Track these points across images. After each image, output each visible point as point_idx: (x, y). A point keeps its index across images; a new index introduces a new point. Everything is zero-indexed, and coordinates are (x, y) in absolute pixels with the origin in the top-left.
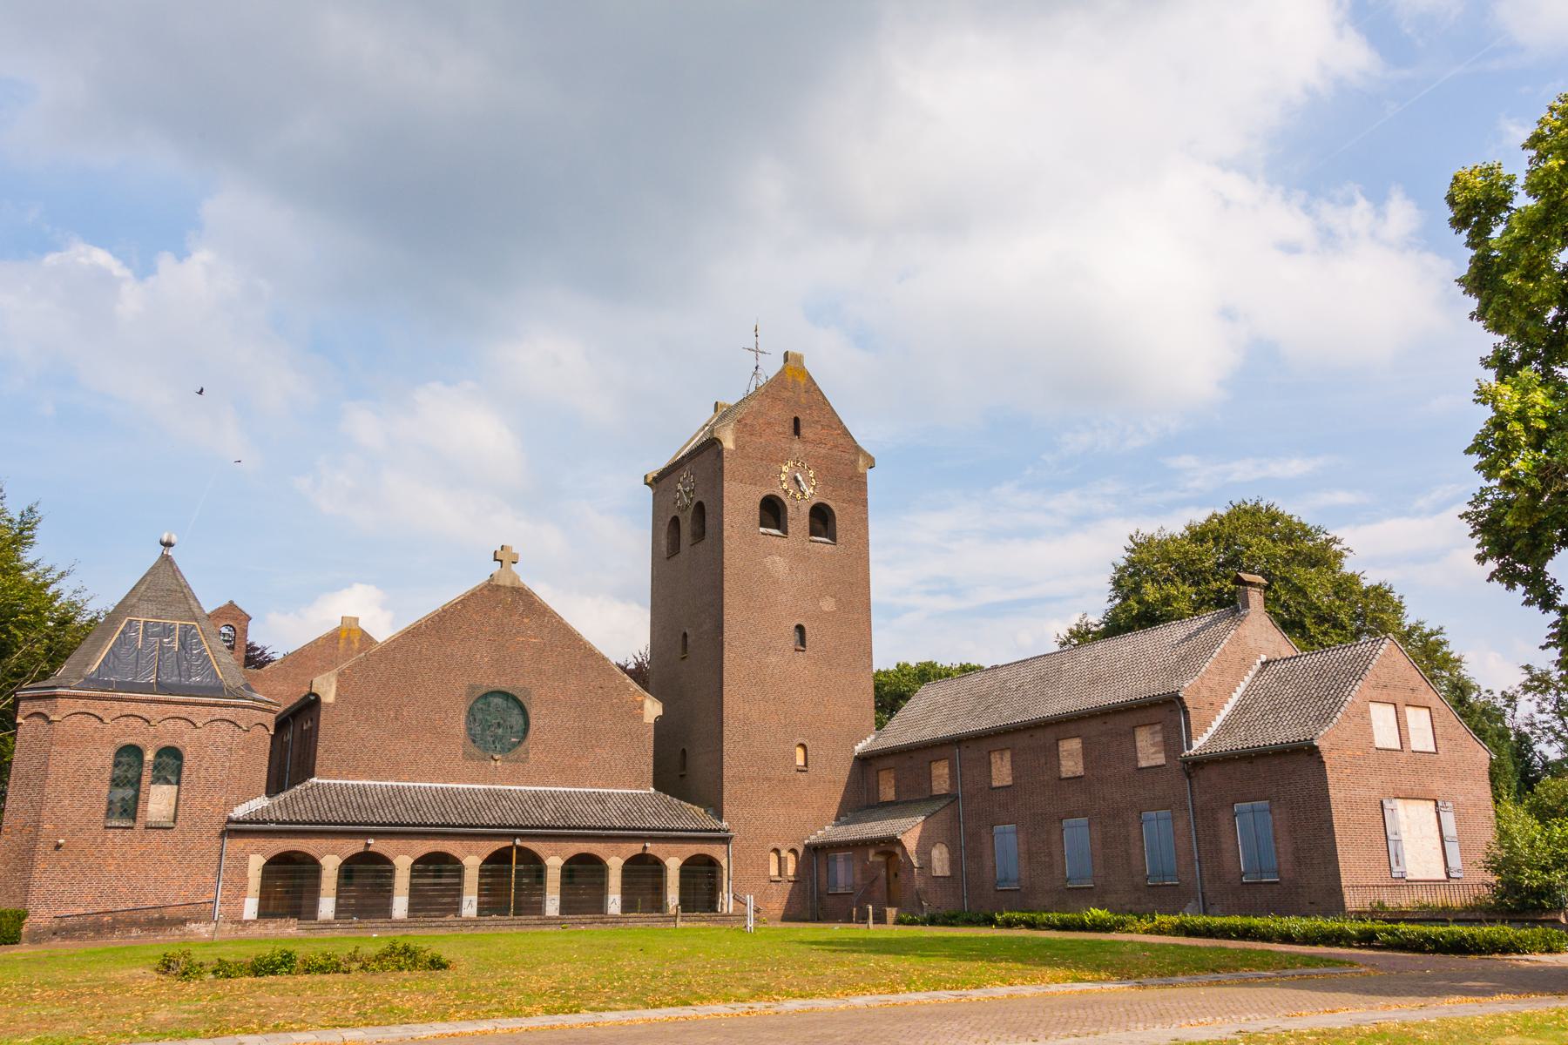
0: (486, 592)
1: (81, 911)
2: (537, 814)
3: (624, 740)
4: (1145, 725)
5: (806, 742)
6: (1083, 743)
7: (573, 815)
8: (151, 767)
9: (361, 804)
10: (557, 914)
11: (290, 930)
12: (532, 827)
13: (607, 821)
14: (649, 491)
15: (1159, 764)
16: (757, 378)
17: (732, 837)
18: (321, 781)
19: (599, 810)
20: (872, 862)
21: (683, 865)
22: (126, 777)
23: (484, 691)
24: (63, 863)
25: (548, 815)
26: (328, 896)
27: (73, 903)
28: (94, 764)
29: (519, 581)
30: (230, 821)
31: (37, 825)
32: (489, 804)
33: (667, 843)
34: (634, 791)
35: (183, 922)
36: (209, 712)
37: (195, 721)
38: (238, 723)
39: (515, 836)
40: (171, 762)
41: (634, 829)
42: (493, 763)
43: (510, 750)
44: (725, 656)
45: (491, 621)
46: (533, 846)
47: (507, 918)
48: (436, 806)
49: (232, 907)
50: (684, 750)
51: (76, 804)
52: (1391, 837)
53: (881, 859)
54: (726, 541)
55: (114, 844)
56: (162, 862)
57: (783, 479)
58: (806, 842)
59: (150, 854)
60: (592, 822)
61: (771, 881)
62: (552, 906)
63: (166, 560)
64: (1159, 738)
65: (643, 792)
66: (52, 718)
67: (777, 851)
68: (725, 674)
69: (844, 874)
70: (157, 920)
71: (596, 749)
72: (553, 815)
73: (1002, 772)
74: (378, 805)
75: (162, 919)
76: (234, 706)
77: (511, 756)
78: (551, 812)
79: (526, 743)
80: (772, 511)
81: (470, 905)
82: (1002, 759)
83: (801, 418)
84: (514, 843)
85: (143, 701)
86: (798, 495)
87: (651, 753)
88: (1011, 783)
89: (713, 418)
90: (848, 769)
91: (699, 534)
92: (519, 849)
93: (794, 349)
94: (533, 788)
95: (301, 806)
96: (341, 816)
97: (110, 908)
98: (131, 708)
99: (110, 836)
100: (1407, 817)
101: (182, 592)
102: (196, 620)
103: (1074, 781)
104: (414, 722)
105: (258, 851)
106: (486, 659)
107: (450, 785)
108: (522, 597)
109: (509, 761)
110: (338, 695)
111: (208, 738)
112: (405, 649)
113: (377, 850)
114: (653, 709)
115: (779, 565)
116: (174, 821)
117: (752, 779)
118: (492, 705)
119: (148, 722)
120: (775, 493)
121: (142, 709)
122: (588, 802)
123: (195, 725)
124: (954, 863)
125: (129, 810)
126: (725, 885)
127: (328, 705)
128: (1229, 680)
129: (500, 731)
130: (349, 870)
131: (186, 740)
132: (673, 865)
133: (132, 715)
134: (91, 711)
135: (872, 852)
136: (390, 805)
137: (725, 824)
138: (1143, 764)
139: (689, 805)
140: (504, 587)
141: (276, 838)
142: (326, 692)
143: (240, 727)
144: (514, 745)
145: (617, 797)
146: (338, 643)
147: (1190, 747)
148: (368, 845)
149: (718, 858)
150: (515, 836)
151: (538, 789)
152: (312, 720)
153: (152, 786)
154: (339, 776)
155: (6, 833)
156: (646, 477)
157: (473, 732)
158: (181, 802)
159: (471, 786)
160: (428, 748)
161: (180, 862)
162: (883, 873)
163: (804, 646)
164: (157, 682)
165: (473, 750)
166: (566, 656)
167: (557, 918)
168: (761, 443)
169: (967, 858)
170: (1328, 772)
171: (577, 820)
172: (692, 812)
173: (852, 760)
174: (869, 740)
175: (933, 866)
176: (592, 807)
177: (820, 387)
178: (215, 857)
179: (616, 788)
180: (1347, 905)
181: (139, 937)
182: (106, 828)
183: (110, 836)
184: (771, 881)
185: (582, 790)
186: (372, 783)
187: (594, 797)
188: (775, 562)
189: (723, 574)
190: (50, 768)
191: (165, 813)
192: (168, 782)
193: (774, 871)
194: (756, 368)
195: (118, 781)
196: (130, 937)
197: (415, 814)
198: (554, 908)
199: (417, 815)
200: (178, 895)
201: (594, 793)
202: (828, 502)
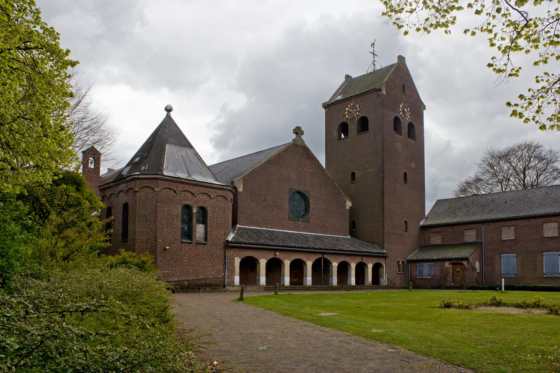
20: (447, 267)
26: (263, 276)
28: (174, 212)
30: (228, 241)
31: (156, 239)
37: (211, 195)
38: (227, 197)
39: (323, 253)
49: (230, 280)
51: (170, 231)
53: (450, 266)
62: (309, 280)
63: (169, 118)
66: (156, 189)
75: (206, 284)
76: (225, 190)
82: (509, 230)
83: (405, 85)
110: (243, 188)
111: (216, 204)
115: (399, 146)
125: (188, 234)
127: (240, 192)
130: (292, 265)
131: (208, 204)
133: (187, 191)
134: (171, 187)
137: (385, 251)
143: (227, 199)
150: (323, 253)
155: (138, 242)
161: (210, 260)
162: (451, 271)
163: (407, 181)
169: (485, 266)
173: (419, 227)
178: (223, 258)
188: (398, 145)
198: (335, 283)
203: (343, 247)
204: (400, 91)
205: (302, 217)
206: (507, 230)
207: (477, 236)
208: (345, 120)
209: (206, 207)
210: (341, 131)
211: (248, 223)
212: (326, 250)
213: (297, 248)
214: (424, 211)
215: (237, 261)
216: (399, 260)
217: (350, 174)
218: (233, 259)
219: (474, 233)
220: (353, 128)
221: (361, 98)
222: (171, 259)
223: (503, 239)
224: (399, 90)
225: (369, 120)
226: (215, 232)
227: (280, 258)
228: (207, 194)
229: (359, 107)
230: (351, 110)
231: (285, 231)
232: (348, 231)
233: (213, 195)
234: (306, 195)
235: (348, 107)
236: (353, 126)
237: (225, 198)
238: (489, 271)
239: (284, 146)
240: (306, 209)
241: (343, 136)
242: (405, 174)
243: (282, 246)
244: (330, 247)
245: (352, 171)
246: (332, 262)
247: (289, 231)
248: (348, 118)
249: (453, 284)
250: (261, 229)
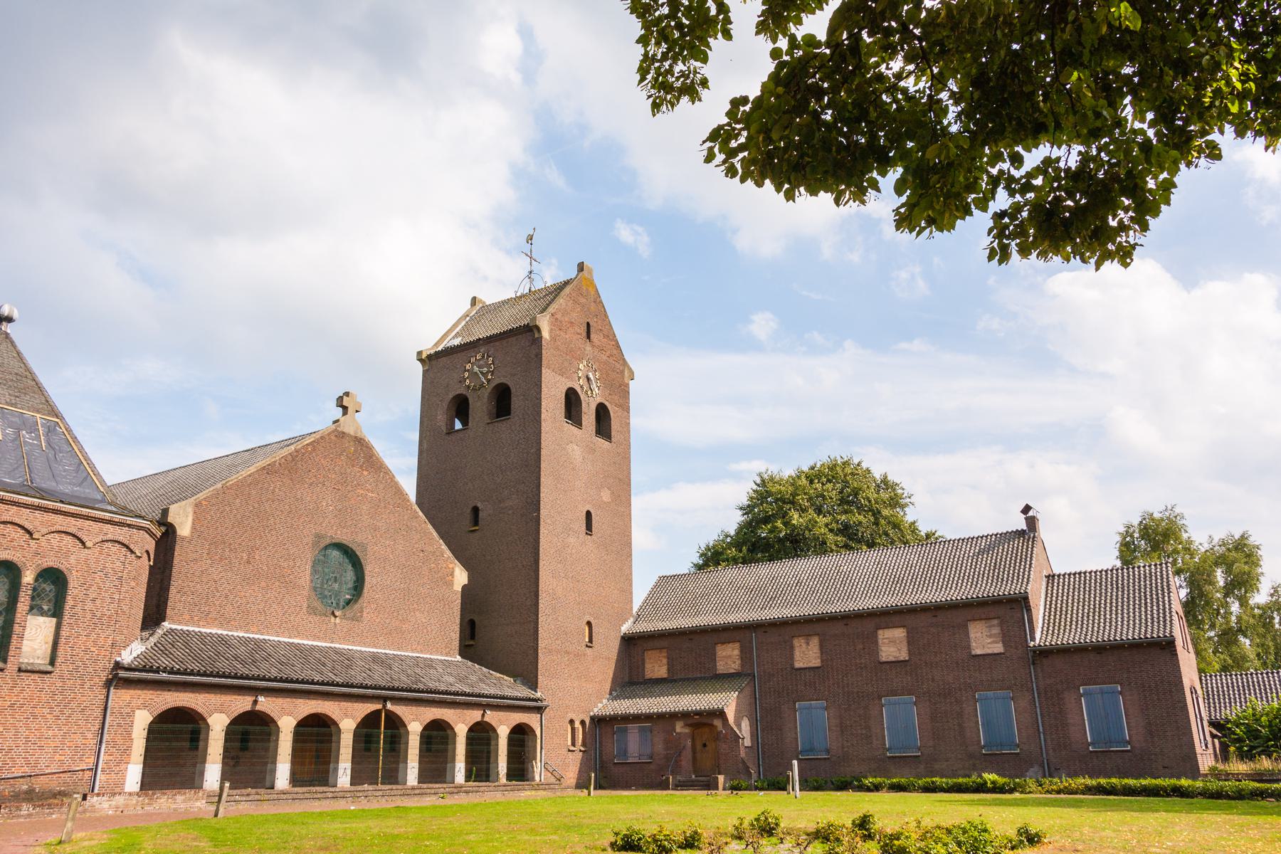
4: (981, 619)
6: (908, 633)
8: (30, 592)
11: (198, 804)
14: (419, 368)
15: (996, 652)
16: (531, 282)
21: (510, 733)
30: (118, 666)
33: (500, 711)
36: (101, 530)
37: (85, 539)
38: (132, 547)
39: (385, 699)
42: (333, 618)
46: (399, 710)
49: (113, 776)
53: (687, 730)
54: (543, 423)
56: (35, 717)
58: (592, 714)
59: (22, 706)
64: (996, 631)
69: (634, 745)
70: (27, 792)
71: (417, 613)
76: (129, 526)
77: (349, 613)
81: (213, 773)
82: (808, 644)
84: (384, 706)
85: (26, 506)
88: (819, 665)
90: (617, 647)
103: (898, 664)
110: (194, 528)
111: (97, 561)
112: (260, 485)
116: (52, 663)
117: (558, 652)
121: (24, 517)
123: (83, 543)
127: (183, 539)
131: (72, 561)
137: (538, 695)
141: (164, 690)
143: (132, 552)
150: (385, 699)
153: (29, 617)
154: (191, 621)
156: (419, 353)
158: (62, 640)
161: (57, 718)
162: (689, 743)
165: (317, 604)
166: (396, 515)
169: (763, 730)
173: (619, 638)
177: (603, 301)
178: (98, 713)
181: (30, 815)
188: (573, 450)
192: (43, 613)
196: (19, 816)
200: (52, 760)
203: (437, 684)
204: (581, 334)
205: (344, 608)
206: (804, 646)
207: (742, 659)
208: (462, 391)
210: (454, 414)
211: (196, 618)
212: (393, 689)
213: (317, 683)
214: (627, 592)
215: (142, 720)
216: (571, 716)
217: (469, 511)
218: (131, 715)
219: (737, 652)
220: (480, 407)
221: (497, 343)
223: (797, 665)
224: (578, 334)
225: (513, 390)
226: (85, 638)
227: (269, 712)
228: (74, 536)
229: (493, 363)
230: (476, 369)
231: (296, 641)
232: (456, 643)
233: (92, 532)
234: (358, 553)
235: (470, 362)
236: (479, 404)
237: (127, 547)
238: (772, 744)
239: (314, 435)
240: (355, 588)
241: (458, 425)
242: (588, 514)
243: (275, 680)
244: (405, 681)
245: (474, 505)
246: (406, 723)
247: (306, 642)
248: (468, 387)
249: (693, 776)
250: (230, 633)
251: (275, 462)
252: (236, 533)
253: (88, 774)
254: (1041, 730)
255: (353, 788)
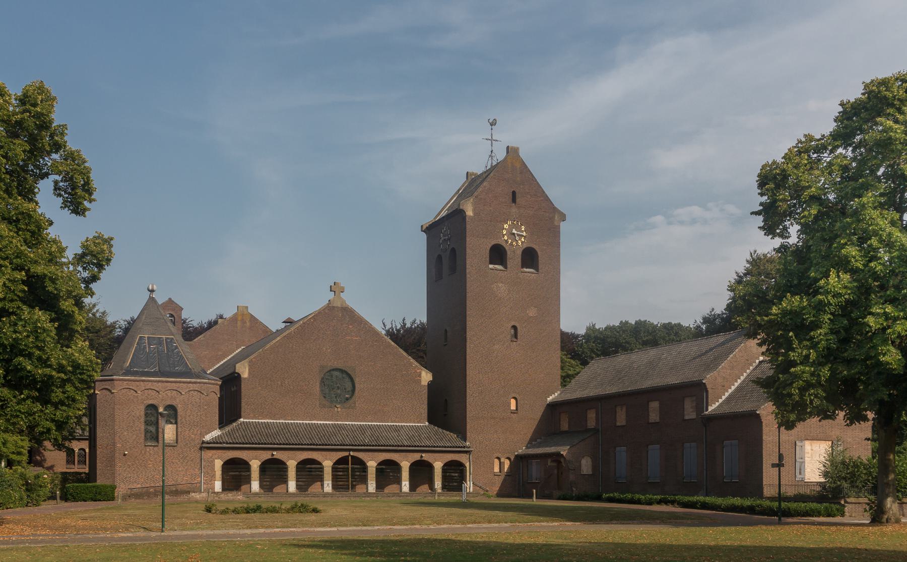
0: (326, 311)
1: (139, 486)
2: (361, 438)
3: (410, 395)
5: (517, 396)
7: (381, 439)
9: (267, 433)
10: (375, 491)
11: (239, 497)
12: (359, 445)
13: (400, 442)
14: (424, 236)
17: (471, 451)
18: (245, 420)
19: (396, 436)
22: (151, 421)
23: (329, 369)
24: (128, 463)
25: (367, 439)
27: (135, 482)
28: (135, 414)
29: (345, 303)
30: (203, 442)
31: (114, 444)
32: (335, 433)
34: (416, 424)
35: (188, 492)
37: (181, 391)
39: (350, 450)
40: (172, 413)
41: (415, 446)
42: (336, 409)
43: (345, 402)
44: (468, 346)
45: (331, 328)
46: (360, 455)
47: (348, 493)
48: (306, 434)
50: (446, 400)
52: (798, 460)
53: (554, 464)
54: (468, 276)
55: (150, 454)
57: (505, 233)
60: (392, 443)
61: (495, 475)
64: (694, 404)
65: (422, 425)
67: (499, 458)
68: (468, 357)
72: (370, 438)
73: (621, 419)
74: (276, 433)
78: (369, 437)
79: (354, 398)
80: (498, 254)
82: (622, 410)
83: (517, 191)
84: (350, 454)
86: (514, 243)
87: (426, 402)
88: (625, 424)
89: (465, 183)
91: (453, 269)
92: (352, 457)
93: (512, 144)
94: (359, 423)
95: (237, 435)
96: (258, 440)
97: (152, 485)
98: (149, 385)
99: (148, 450)
100: (812, 450)
101: (164, 319)
102: (173, 335)
104: (292, 387)
105: (218, 458)
106: (329, 350)
107: (313, 422)
108: (347, 312)
109: (345, 408)
110: (250, 373)
113: (278, 457)
114: (426, 377)
115: (501, 289)
116: (177, 443)
118: (334, 376)
119: (159, 392)
120: (500, 243)
122: (390, 431)
124: (595, 467)
125: (154, 436)
126: (468, 477)
128: (737, 372)
129: (339, 391)
132: (438, 466)
134: (131, 387)
135: (549, 461)
136: (282, 433)
138: (687, 417)
139: (448, 433)
140: (337, 307)
142: (243, 372)
143: (203, 394)
144: (347, 399)
145: (407, 428)
146: (237, 323)
147: (707, 410)
148: (273, 455)
149: (463, 462)
150: (350, 450)
151: (362, 423)
152: (236, 386)
156: (422, 226)
157: (324, 392)
158: (179, 433)
159: (325, 422)
160: (300, 402)
162: (556, 471)
163: (517, 339)
164: (159, 371)
167: (374, 493)
168: (491, 210)
170: (764, 427)
171: (383, 442)
172: (449, 436)
174: (556, 394)
175: (582, 468)
176: (392, 434)
178: (198, 460)
179: (406, 423)
180: (765, 494)
182: (145, 446)
183: (148, 450)
184: (495, 475)
185: (386, 424)
186: (272, 421)
187: (394, 428)
189: (466, 296)
190: (116, 417)
191: (172, 438)
192: (171, 423)
193: (497, 469)
194: (492, 152)
195: (147, 422)
197: (296, 438)
198: (372, 488)
199: (297, 439)
201: (393, 425)
202: (534, 246)
209: (175, 405)
215: (218, 464)
218: (213, 461)
222: (133, 465)
251: (291, 332)
252: (273, 372)
253: (198, 485)
254: (705, 471)
255: (410, 493)
